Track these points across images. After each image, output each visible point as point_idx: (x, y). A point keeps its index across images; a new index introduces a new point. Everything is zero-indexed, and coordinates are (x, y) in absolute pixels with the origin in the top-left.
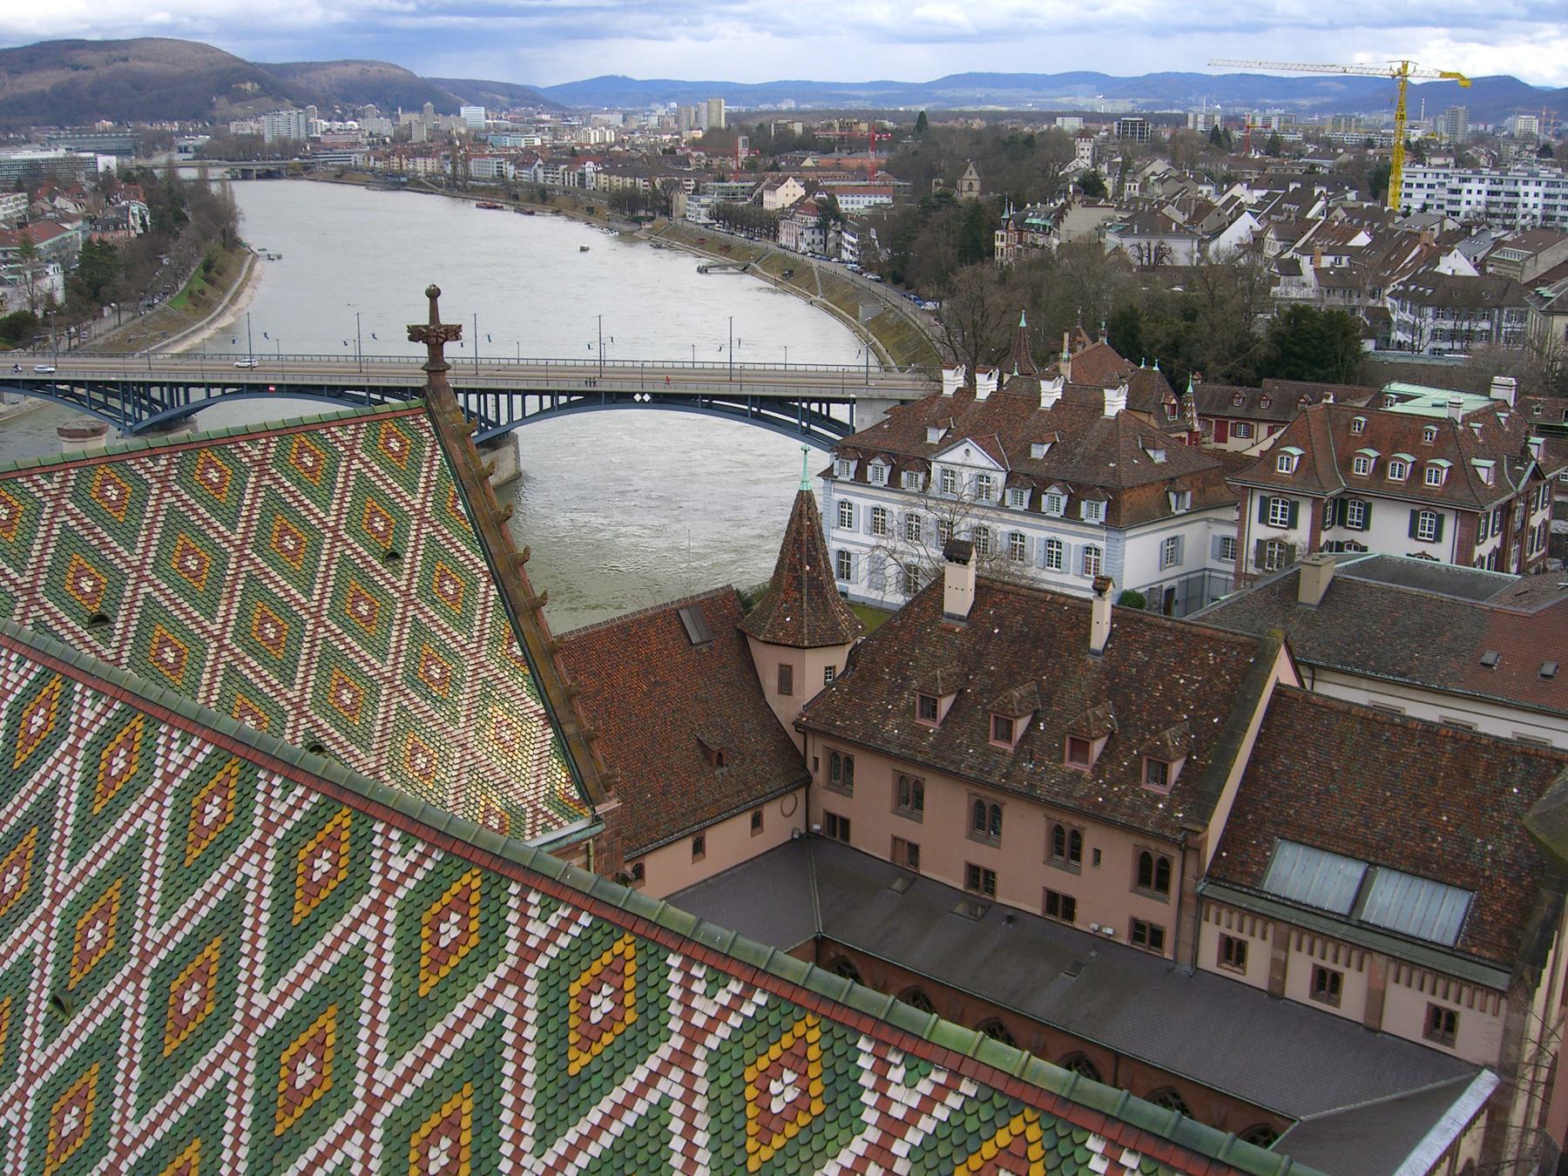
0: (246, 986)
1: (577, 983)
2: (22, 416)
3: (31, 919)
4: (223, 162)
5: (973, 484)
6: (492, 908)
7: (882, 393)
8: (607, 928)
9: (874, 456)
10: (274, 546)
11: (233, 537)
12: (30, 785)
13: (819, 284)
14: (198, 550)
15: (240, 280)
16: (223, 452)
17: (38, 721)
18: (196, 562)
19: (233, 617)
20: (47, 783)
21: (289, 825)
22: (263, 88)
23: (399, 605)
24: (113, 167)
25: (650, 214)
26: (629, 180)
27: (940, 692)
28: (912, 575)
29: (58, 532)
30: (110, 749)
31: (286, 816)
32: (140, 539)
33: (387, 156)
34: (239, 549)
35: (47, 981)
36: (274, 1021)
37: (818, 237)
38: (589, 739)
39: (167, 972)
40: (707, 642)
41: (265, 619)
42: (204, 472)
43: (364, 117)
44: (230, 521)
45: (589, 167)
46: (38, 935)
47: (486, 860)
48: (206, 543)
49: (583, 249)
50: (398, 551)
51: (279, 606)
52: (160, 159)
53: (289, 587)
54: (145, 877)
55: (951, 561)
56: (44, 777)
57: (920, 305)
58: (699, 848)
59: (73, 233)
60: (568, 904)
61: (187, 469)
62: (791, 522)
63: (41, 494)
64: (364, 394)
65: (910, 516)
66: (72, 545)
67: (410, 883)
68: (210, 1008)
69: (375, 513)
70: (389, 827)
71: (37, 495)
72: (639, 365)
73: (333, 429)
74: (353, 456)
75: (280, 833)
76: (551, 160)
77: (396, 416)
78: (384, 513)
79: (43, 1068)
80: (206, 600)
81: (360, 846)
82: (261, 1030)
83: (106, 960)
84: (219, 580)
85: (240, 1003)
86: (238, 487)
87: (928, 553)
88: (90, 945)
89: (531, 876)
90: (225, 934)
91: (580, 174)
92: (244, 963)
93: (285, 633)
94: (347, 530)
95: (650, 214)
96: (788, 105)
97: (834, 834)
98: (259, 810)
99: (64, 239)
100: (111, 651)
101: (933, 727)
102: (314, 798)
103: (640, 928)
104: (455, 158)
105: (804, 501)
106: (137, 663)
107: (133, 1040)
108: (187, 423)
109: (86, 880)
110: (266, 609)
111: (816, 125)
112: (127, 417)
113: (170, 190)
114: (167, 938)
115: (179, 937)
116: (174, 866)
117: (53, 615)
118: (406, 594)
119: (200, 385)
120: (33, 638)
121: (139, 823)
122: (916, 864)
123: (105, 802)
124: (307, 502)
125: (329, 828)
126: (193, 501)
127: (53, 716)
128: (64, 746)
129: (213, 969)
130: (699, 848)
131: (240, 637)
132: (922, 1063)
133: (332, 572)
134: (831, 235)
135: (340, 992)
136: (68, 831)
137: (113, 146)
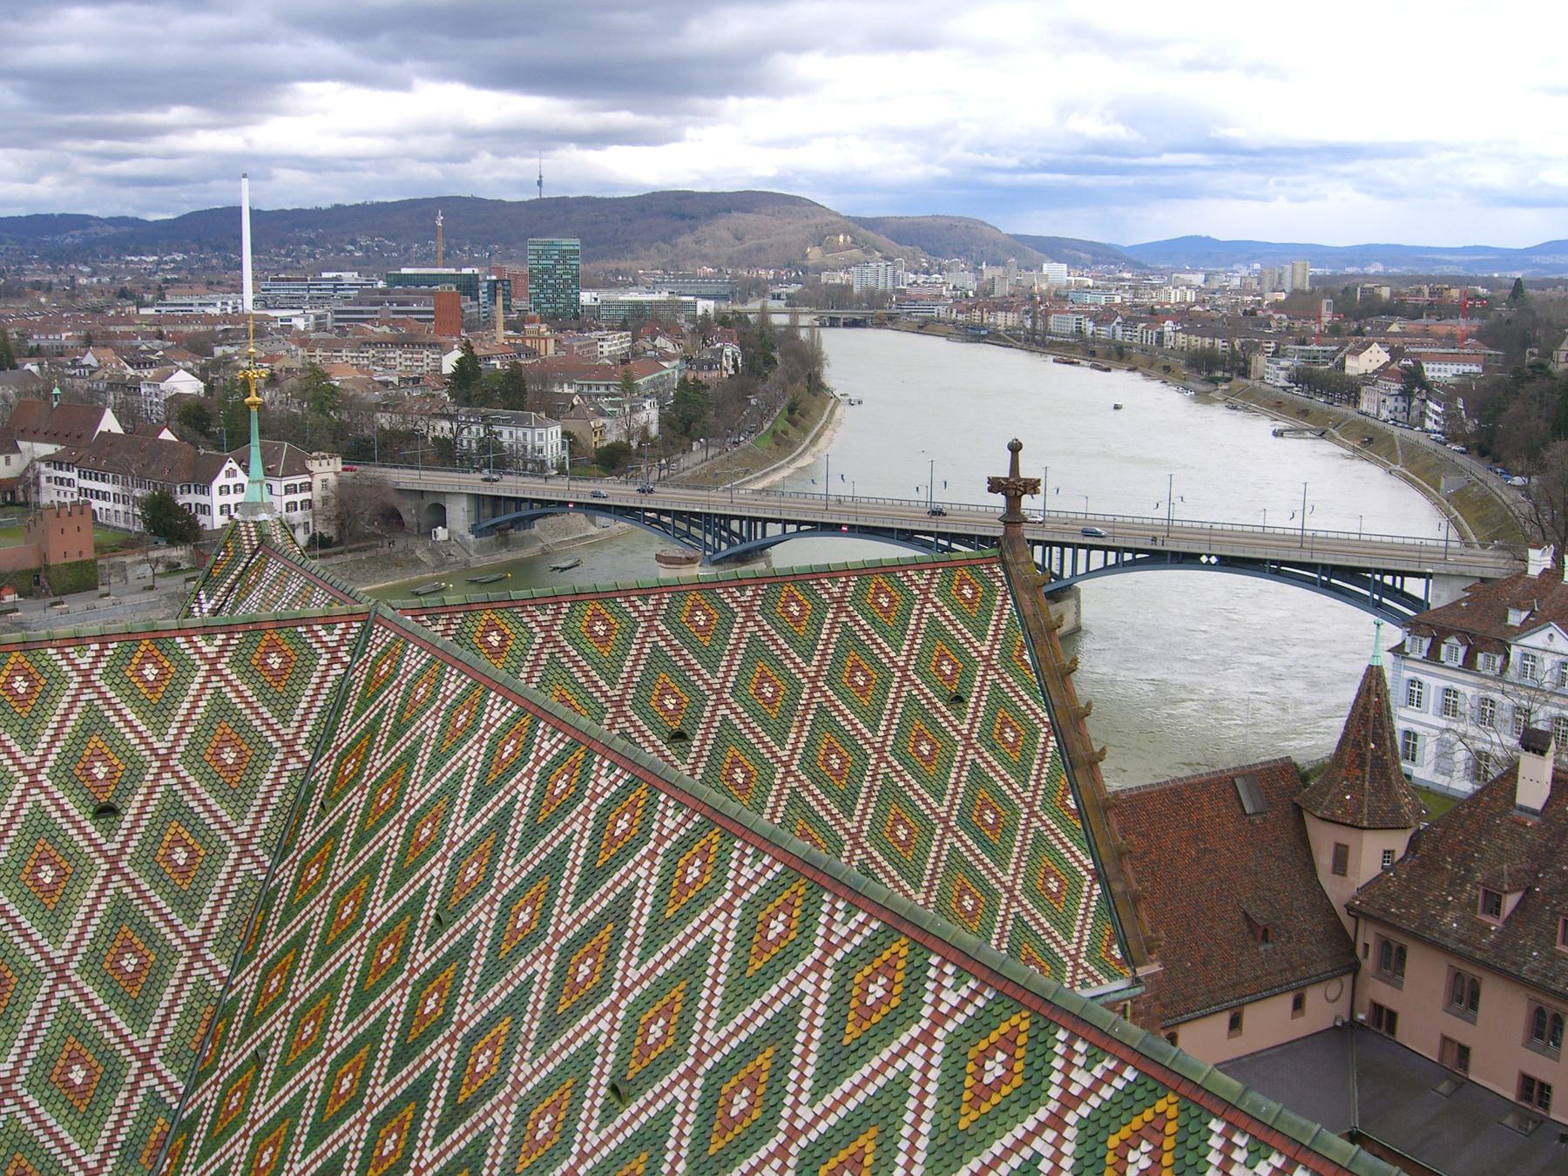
0: (793, 1098)
1: (1117, 1136)
2: (610, 540)
3: (599, 1009)
5: (1556, 671)
6: (1038, 1052)
7: (1461, 569)
8: (1151, 1085)
9: (1449, 633)
10: (845, 680)
11: (808, 669)
12: (609, 883)
13: (1399, 452)
15: (822, 423)
18: (771, 690)
20: (626, 883)
23: (960, 748)
24: (711, 311)
25: (1227, 375)
26: (1208, 340)
27: (1506, 887)
28: (1483, 763)
30: (686, 858)
32: (723, 663)
33: (969, 309)
34: (813, 680)
35: (607, 1069)
36: (816, 1134)
37: (1401, 405)
38: (1136, 900)
39: (720, 1074)
40: (1262, 813)
43: (949, 271)
45: (1168, 326)
46: (604, 1024)
47: (1035, 1005)
48: (782, 672)
49: (1117, 407)
50: (963, 695)
52: (754, 305)
53: (857, 721)
54: (708, 982)
55: (1527, 750)
56: (623, 877)
57: (1506, 479)
58: (1235, 1024)
59: (670, 371)
60: (1113, 1057)
62: (1358, 696)
63: (636, 614)
64: (932, 539)
65: (1484, 700)
66: (660, 665)
67: (960, 1018)
68: (756, 1114)
69: (943, 656)
70: (945, 960)
72: (1208, 526)
73: (909, 573)
74: (927, 600)
75: (839, 955)
76: (1129, 318)
77: (970, 563)
79: (596, 1150)
81: (914, 976)
82: (803, 1142)
83: (664, 1056)
84: (791, 710)
85: (786, 1112)
86: (816, 622)
87: (1502, 741)
88: (651, 1040)
89: (1079, 1024)
90: (778, 1045)
91: (1159, 333)
92: (793, 1075)
94: (916, 671)
95: (1227, 375)
96: (1375, 268)
97: (1379, 1026)
98: (821, 930)
100: (687, 766)
101: (1495, 924)
102: (875, 925)
103: (1184, 1089)
104: (1035, 313)
105: (1373, 677)
106: (709, 780)
107: (681, 1134)
108: (762, 556)
109: (653, 979)
110: (832, 740)
111: (1404, 290)
112: (707, 547)
113: (762, 335)
114: (723, 1042)
115: (734, 1043)
116: (736, 974)
117: (637, 729)
118: (967, 738)
119: (777, 521)
120: (625, 747)
122: (1466, 1068)
123: (677, 907)
125: (886, 955)
126: (773, 632)
128: (644, 851)
129: (764, 1077)
130: (1235, 1024)
131: (806, 765)
134: (1415, 403)
135: (882, 1114)
136: (641, 931)
137: (713, 291)
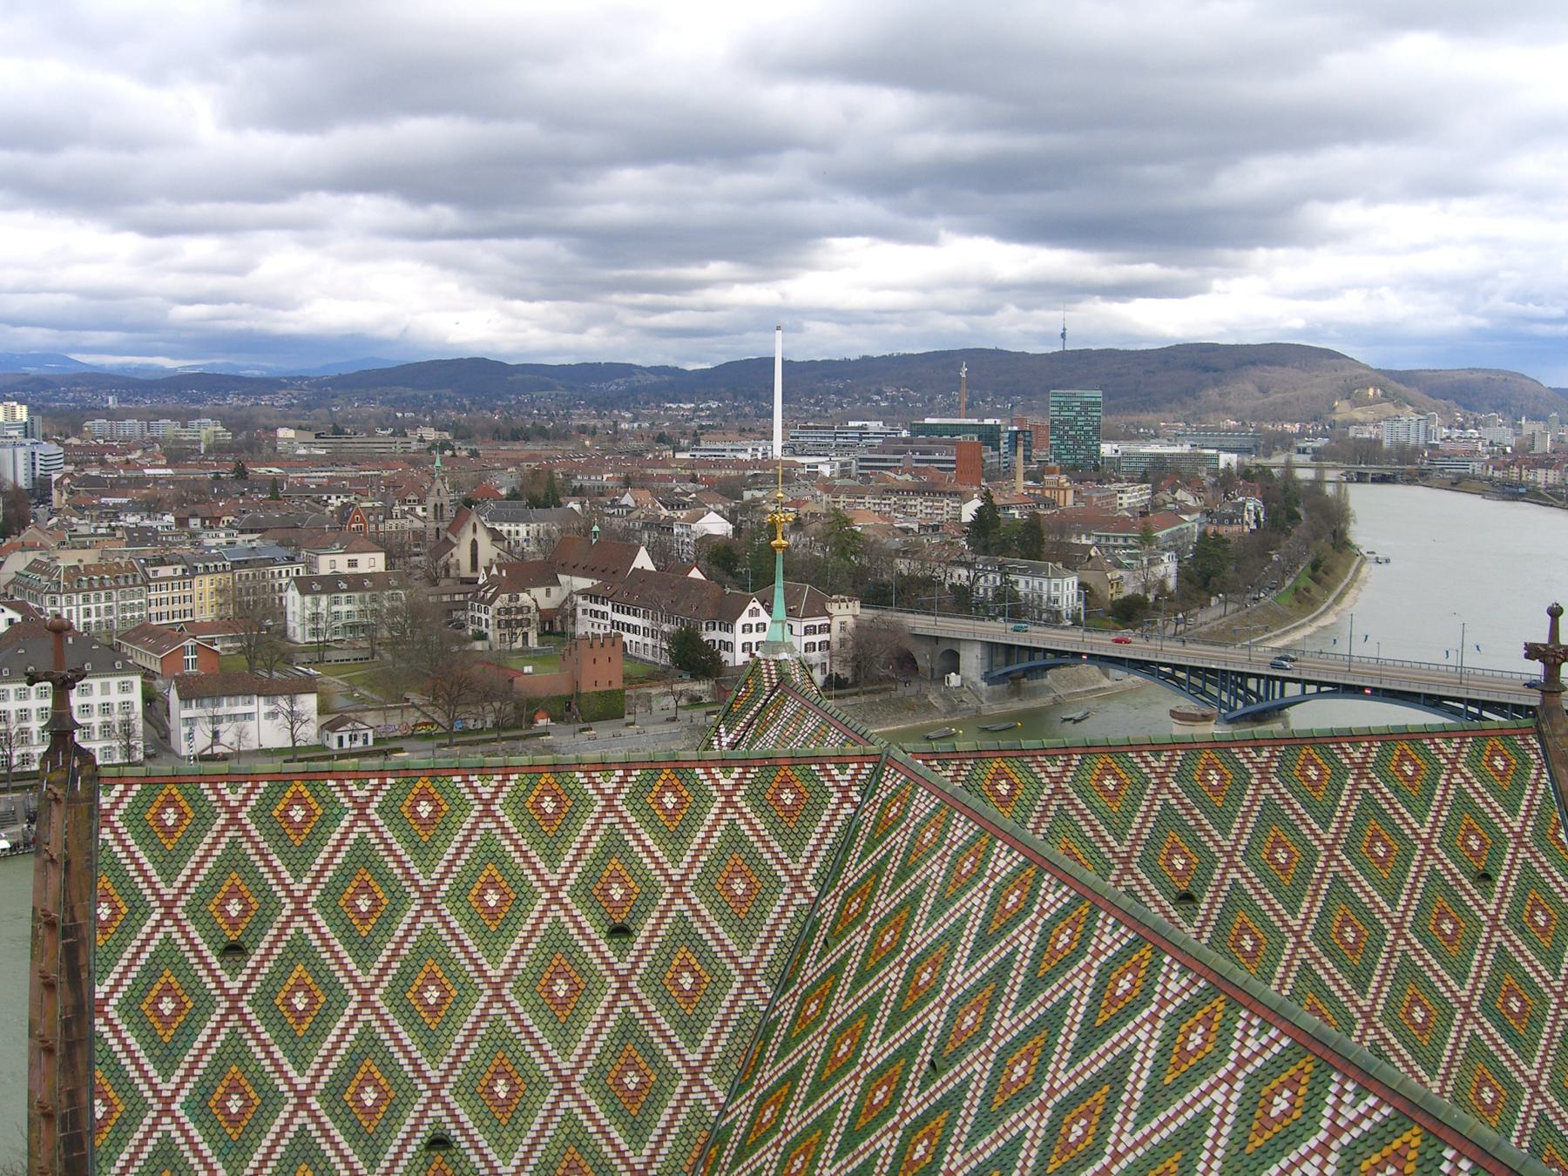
4: (1340, 464)
11: (1324, 836)
12: (1108, 1044)
14: (1289, 844)
16: (1324, 751)
17: (1125, 984)
19: (1315, 915)
20: (1125, 1045)
21: (1355, 1132)
22: (1385, 395)
23: (1485, 929)
24: (1234, 465)
29: (1159, 808)
31: (1355, 1123)
32: (1235, 825)
33: (1507, 466)
34: (1329, 848)
41: (1346, 921)
42: (1303, 770)
43: (1485, 426)
44: (1323, 820)
48: (1297, 838)
50: (1491, 873)
51: (1362, 911)
52: (1279, 459)
54: (1205, 1155)
56: (1123, 1039)
59: (1190, 525)
61: (1288, 763)
64: (1462, 706)
66: (1171, 823)
69: (1470, 830)
71: (1145, 771)
73: (1437, 740)
74: (1455, 769)
75: (1345, 1139)
77: (1503, 733)
78: (1480, 831)
80: (1290, 894)
84: (1305, 876)
93: (1364, 939)
98: (1327, 1112)
99: (1181, 529)
108: (1279, 716)
110: (1348, 912)
112: (1222, 704)
113: (1286, 489)
116: (1235, 1150)
118: (1494, 919)
121: (1206, 1101)
124: (1403, 810)
125: (1397, 1144)
126: (1290, 796)
127: (1139, 983)
128: (1145, 1013)
131: (1319, 937)
132: (1432, 1137)
133: (1419, 885)
136: (1138, 1095)
